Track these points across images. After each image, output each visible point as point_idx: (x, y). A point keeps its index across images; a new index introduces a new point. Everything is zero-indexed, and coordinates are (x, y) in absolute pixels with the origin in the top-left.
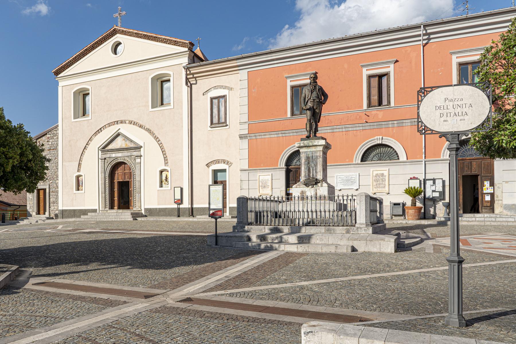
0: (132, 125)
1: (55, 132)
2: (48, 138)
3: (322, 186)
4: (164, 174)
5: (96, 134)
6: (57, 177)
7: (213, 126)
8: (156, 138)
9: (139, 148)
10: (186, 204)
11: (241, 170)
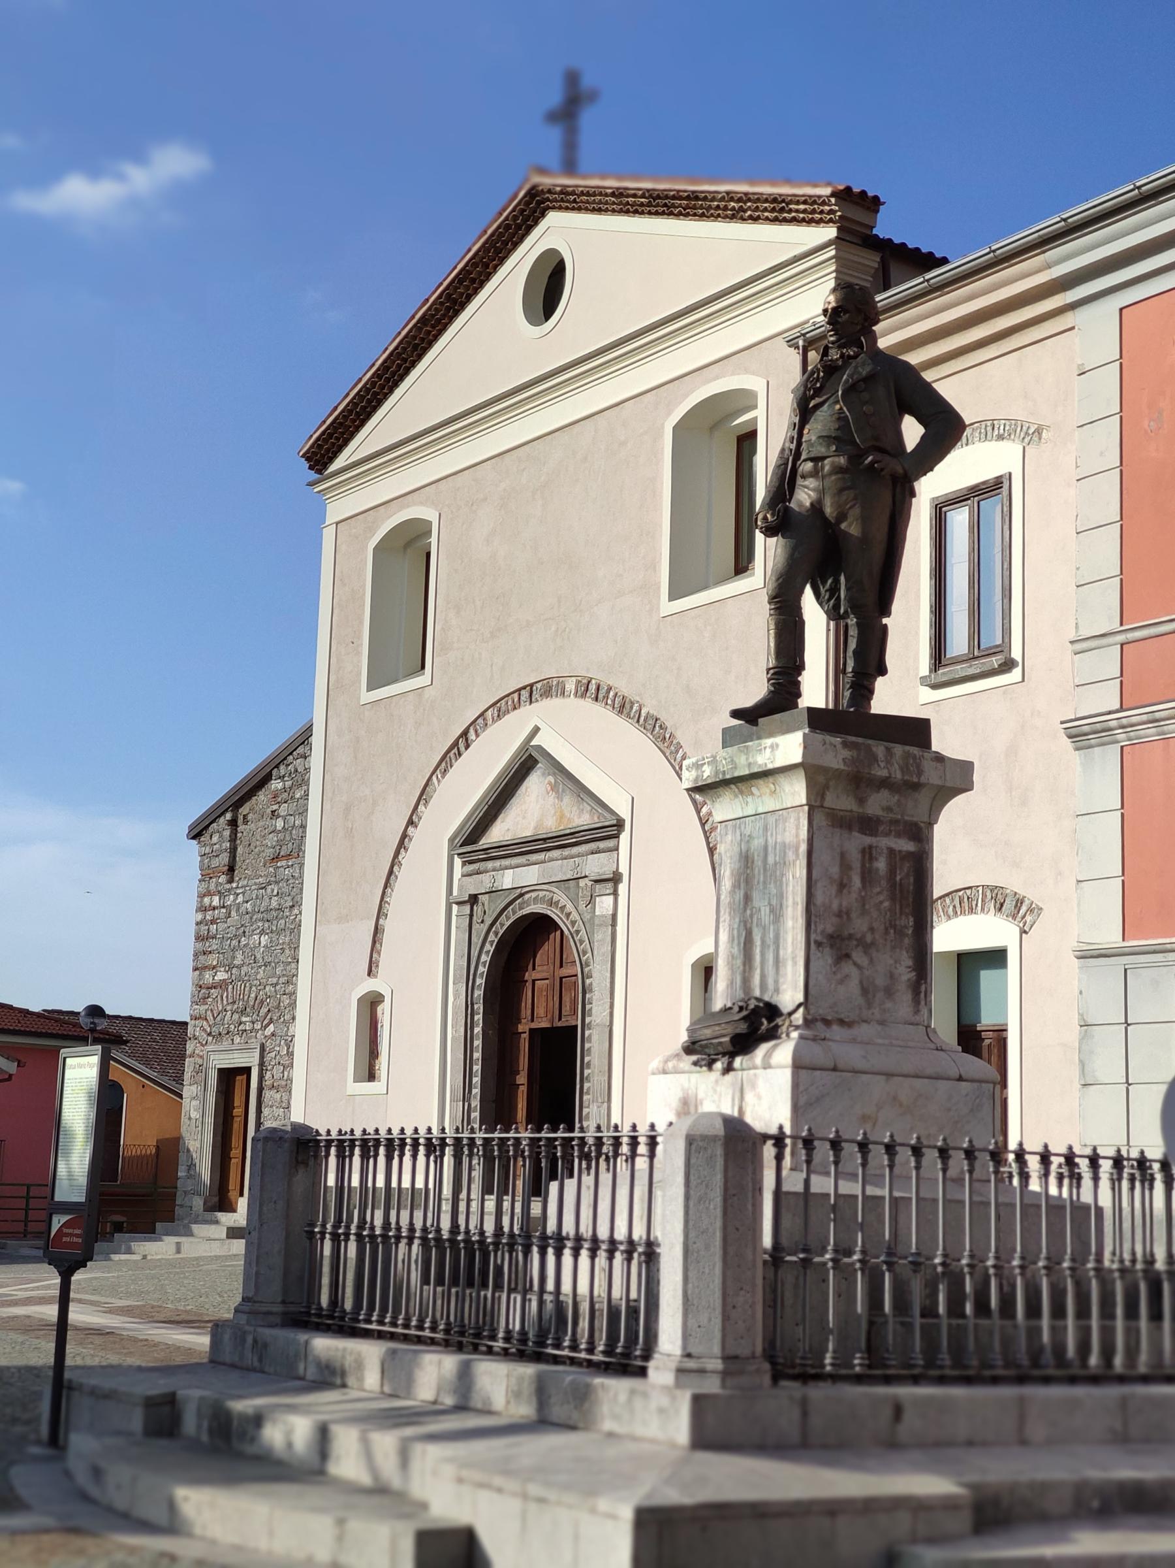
0: (587, 704)
3: (767, 1066)
5: (445, 763)
7: (944, 673)
9: (610, 831)
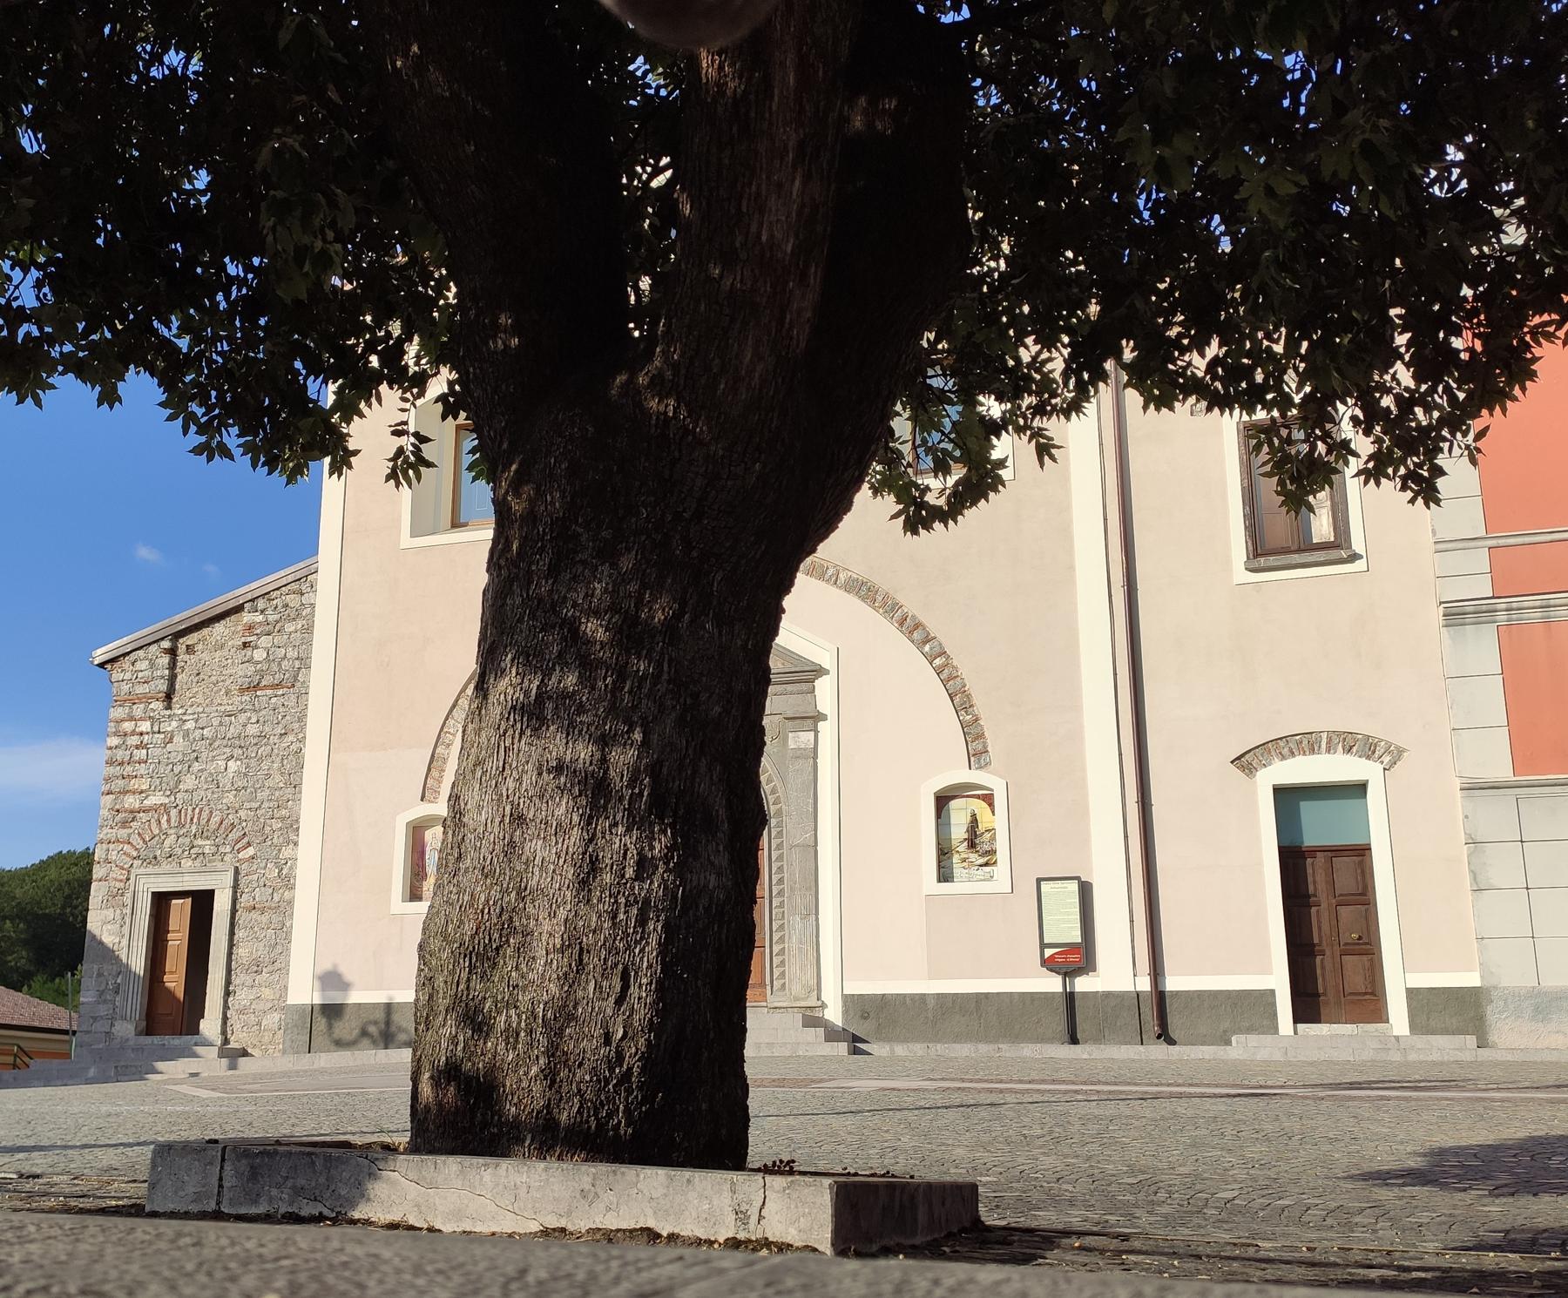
1: (293, 600)
2: (250, 628)
4: (959, 813)
6: (292, 825)
8: (912, 628)
10: (1116, 972)
11: (1471, 788)
